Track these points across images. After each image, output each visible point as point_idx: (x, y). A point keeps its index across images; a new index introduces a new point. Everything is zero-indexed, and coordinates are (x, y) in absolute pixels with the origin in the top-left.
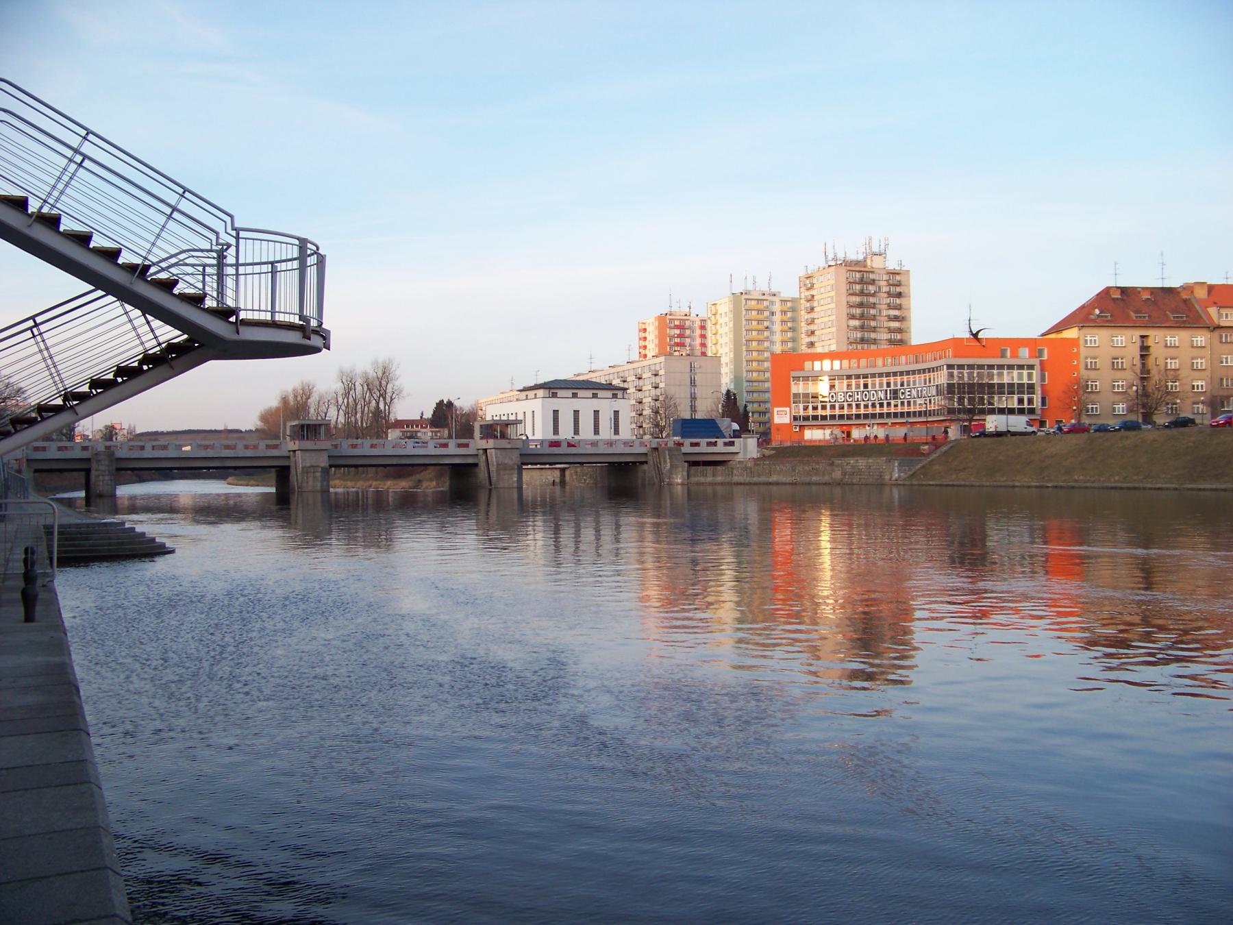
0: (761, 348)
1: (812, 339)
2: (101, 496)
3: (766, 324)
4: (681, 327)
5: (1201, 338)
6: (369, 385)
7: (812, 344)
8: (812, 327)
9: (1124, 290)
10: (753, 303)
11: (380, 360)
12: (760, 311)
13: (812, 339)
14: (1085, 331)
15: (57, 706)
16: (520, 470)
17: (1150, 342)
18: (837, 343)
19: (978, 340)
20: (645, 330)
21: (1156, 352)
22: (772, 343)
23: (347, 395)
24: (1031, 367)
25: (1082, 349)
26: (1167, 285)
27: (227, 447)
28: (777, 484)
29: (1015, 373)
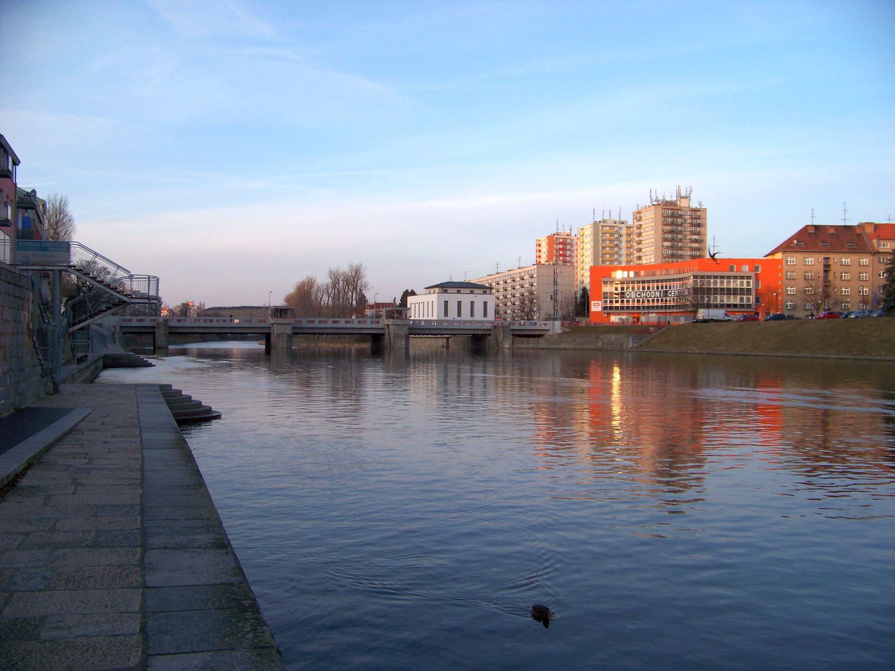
0: (612, 259)
1: (640, 254)
2: (160, 348)
3: (616, 243)
4: (564, 243)
5: (865, 260)
6: (347, 281)
7: (640, 258)
8: (640, 246)
9: (817, 228)
10: (607, 228)
11: (354, 264)
12: (612, 234)
13: (640, 254)
14: (786, 254)
15: (196, 481)
16: (407, 338)
17: (831, 262)
18: (655, 257)
19: (715, 260)
20: (540, 245)
21: (834, 268)
22: (620, 256)
23: (334, 287)
24: (749, 278)
25: (784, 266)
26: (848, 224)
28: (564, 349)
29: (739, 281)
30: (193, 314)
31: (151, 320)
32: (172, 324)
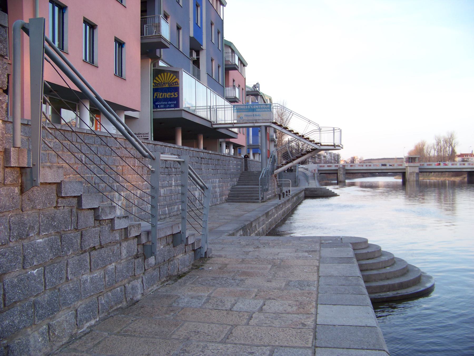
2: (340, 182)
6: (446, 141)
23: (438, 145)
27: (383, 165)
30: (357, 162)
31: (335, 166)
32: (347, 168)
